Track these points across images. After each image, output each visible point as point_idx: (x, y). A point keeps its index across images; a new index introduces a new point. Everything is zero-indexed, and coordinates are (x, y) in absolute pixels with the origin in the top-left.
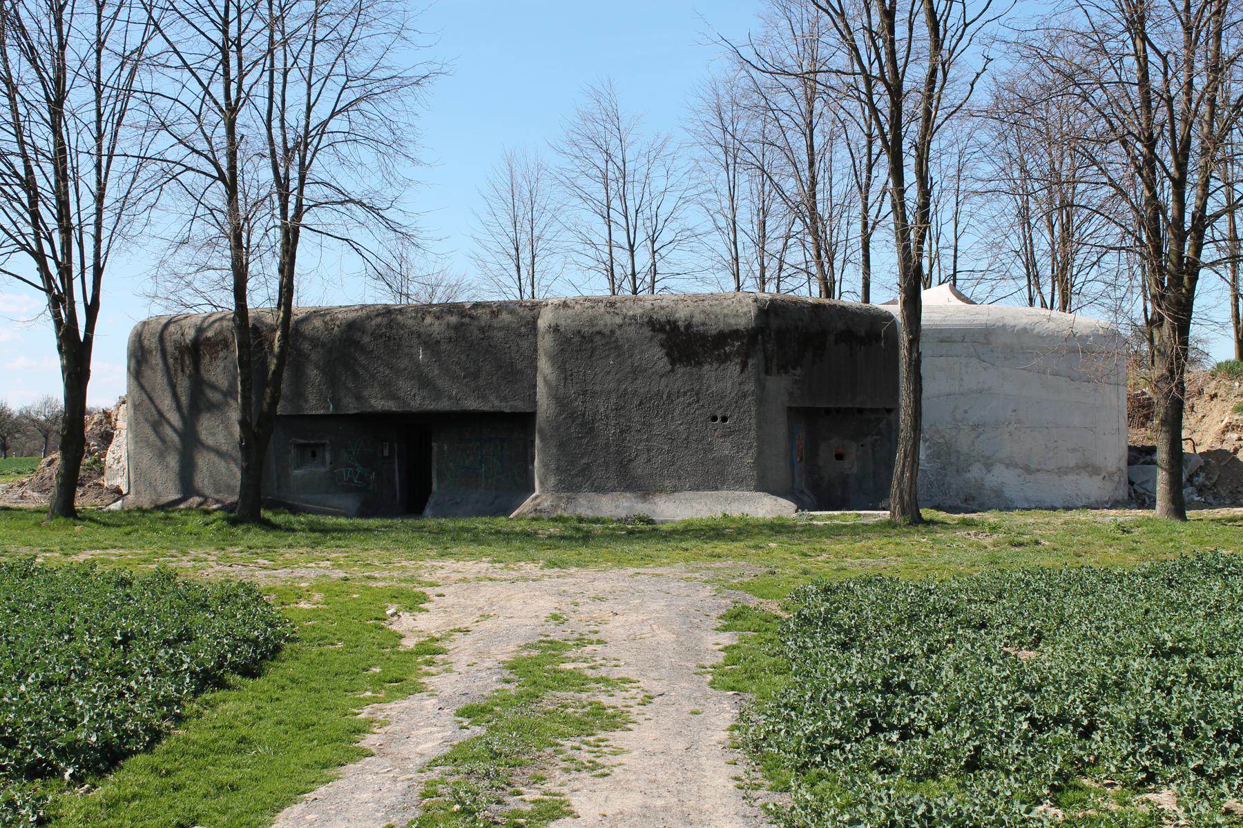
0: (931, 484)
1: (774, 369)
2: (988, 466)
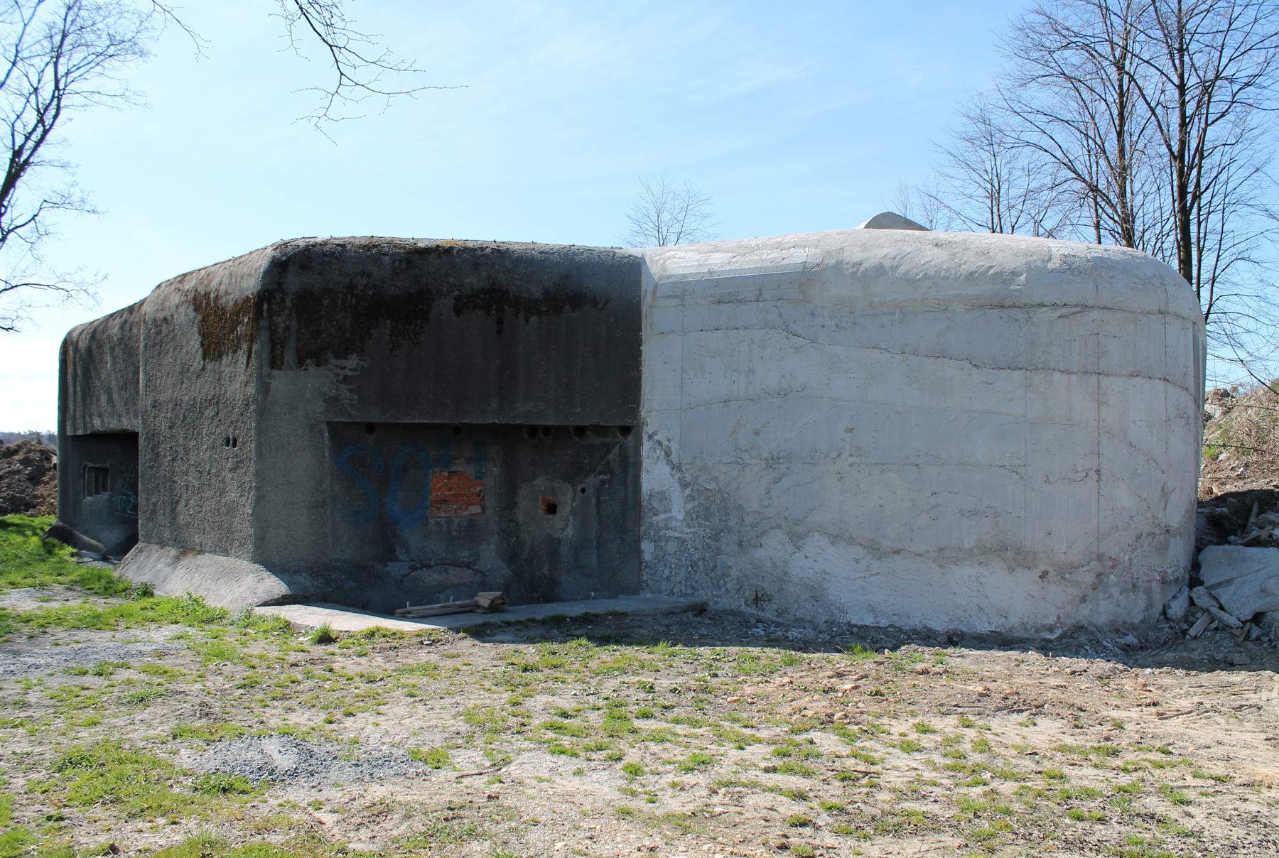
0: (693, 565)
1: (290, 357)
2: (797, 539)
